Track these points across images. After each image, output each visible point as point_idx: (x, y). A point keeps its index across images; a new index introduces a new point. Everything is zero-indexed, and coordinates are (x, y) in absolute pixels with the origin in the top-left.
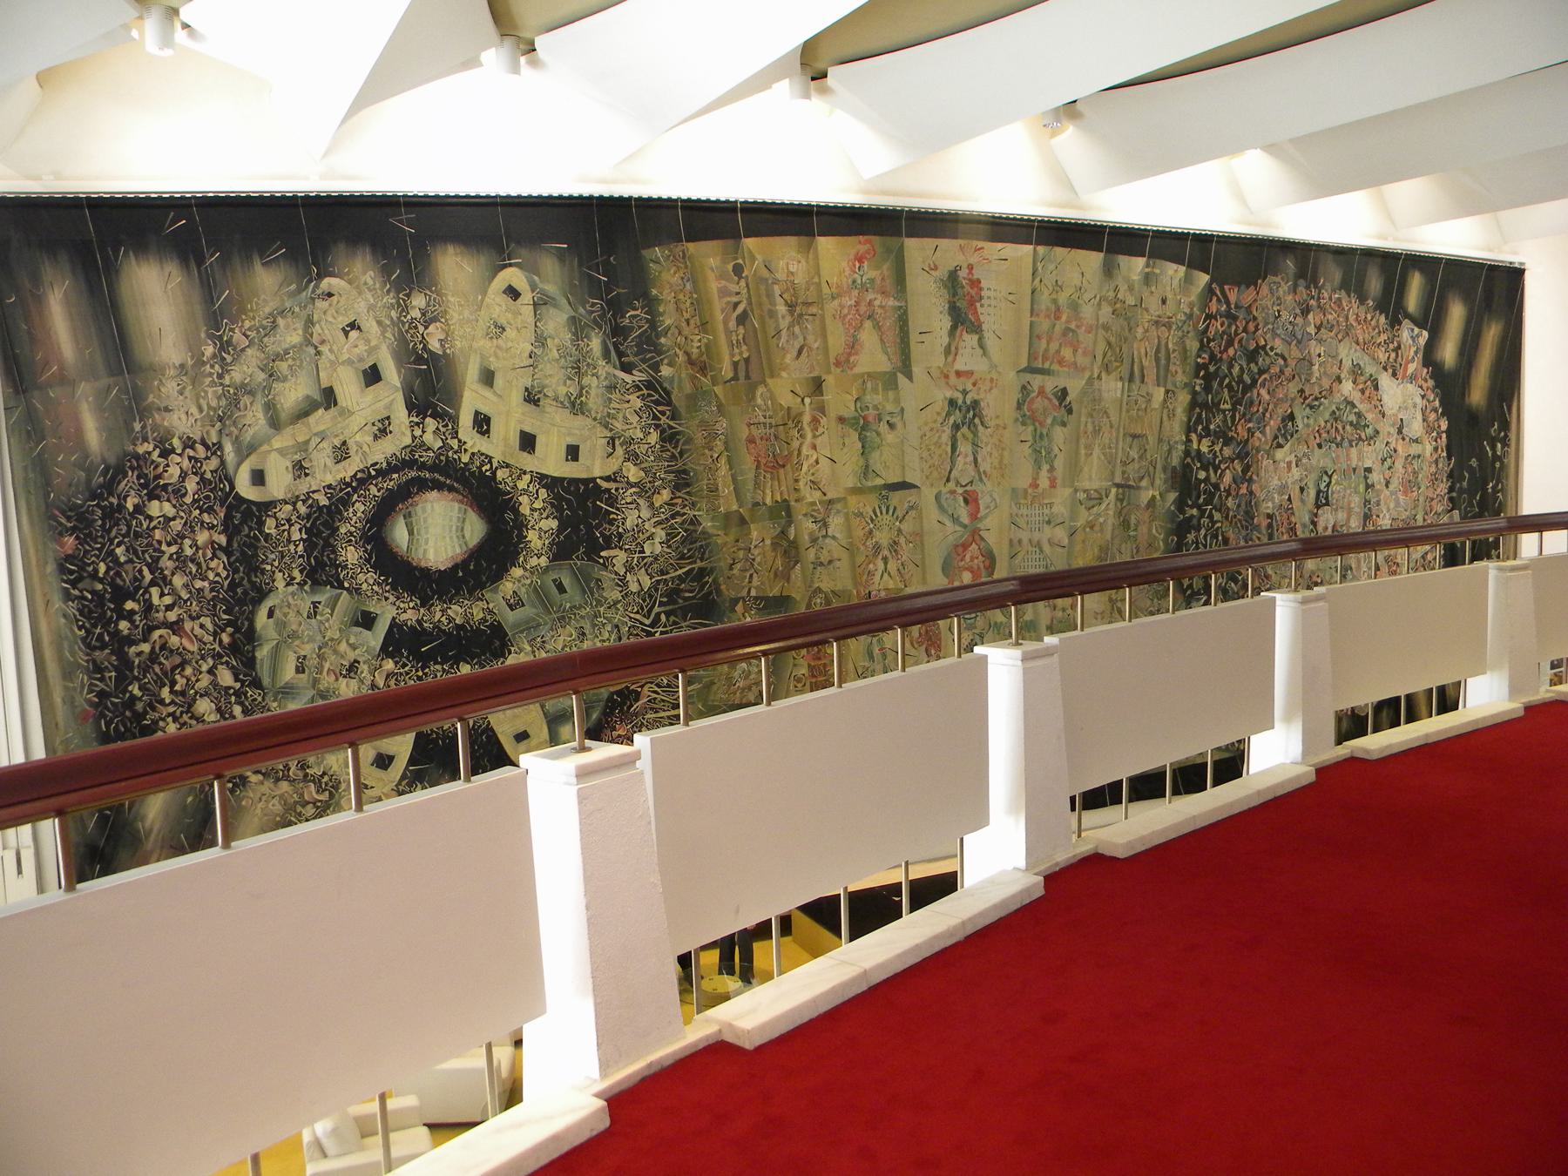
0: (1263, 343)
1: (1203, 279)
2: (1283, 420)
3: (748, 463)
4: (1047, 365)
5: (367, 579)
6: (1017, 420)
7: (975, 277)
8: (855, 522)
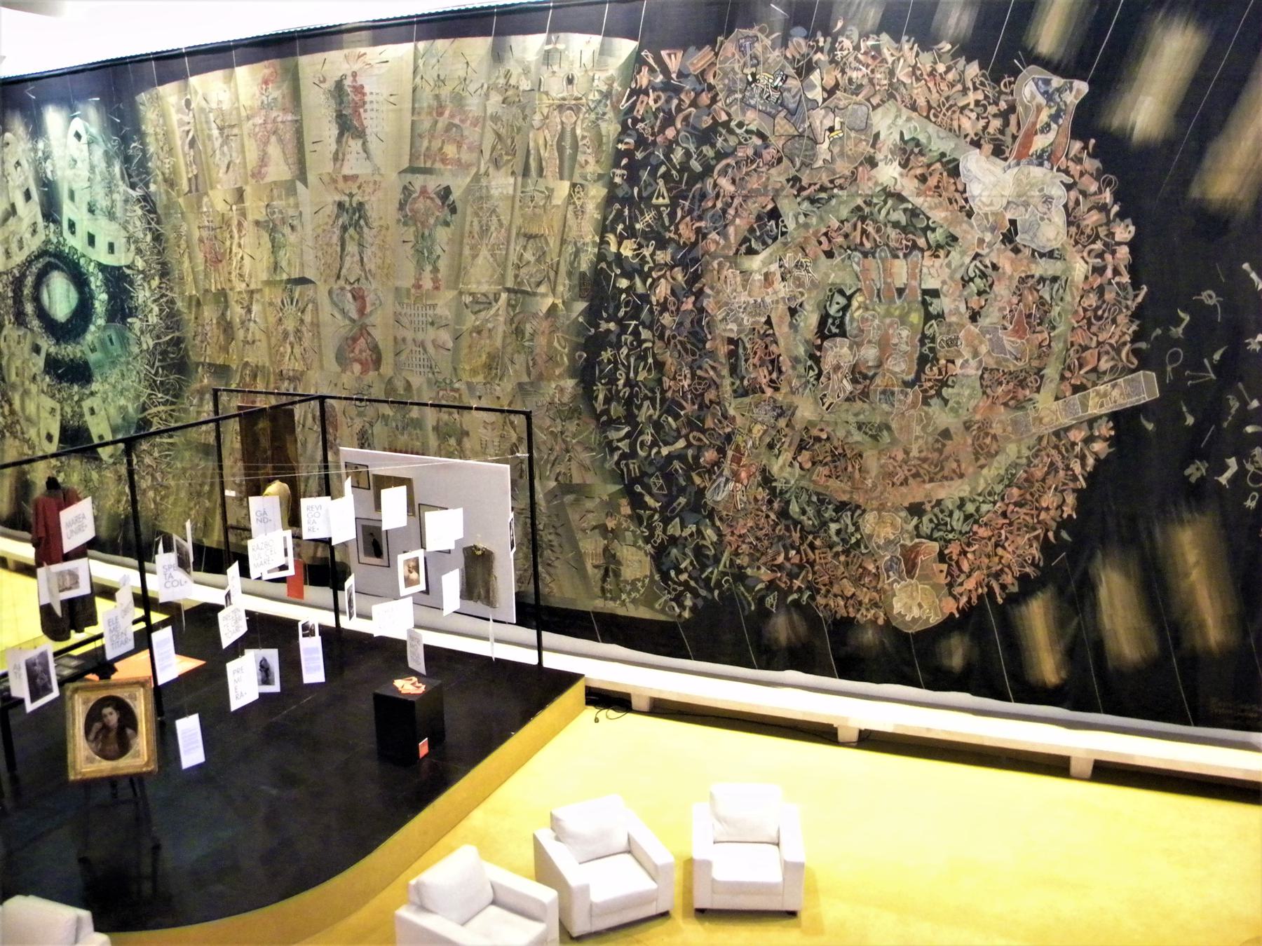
0: (724, 117)
1: (625, 47)
2: (759, 218)
3: (200, 257)
4: (428, 165)
6: (399, 221)
7: (359, 83)
8: (269, 310)
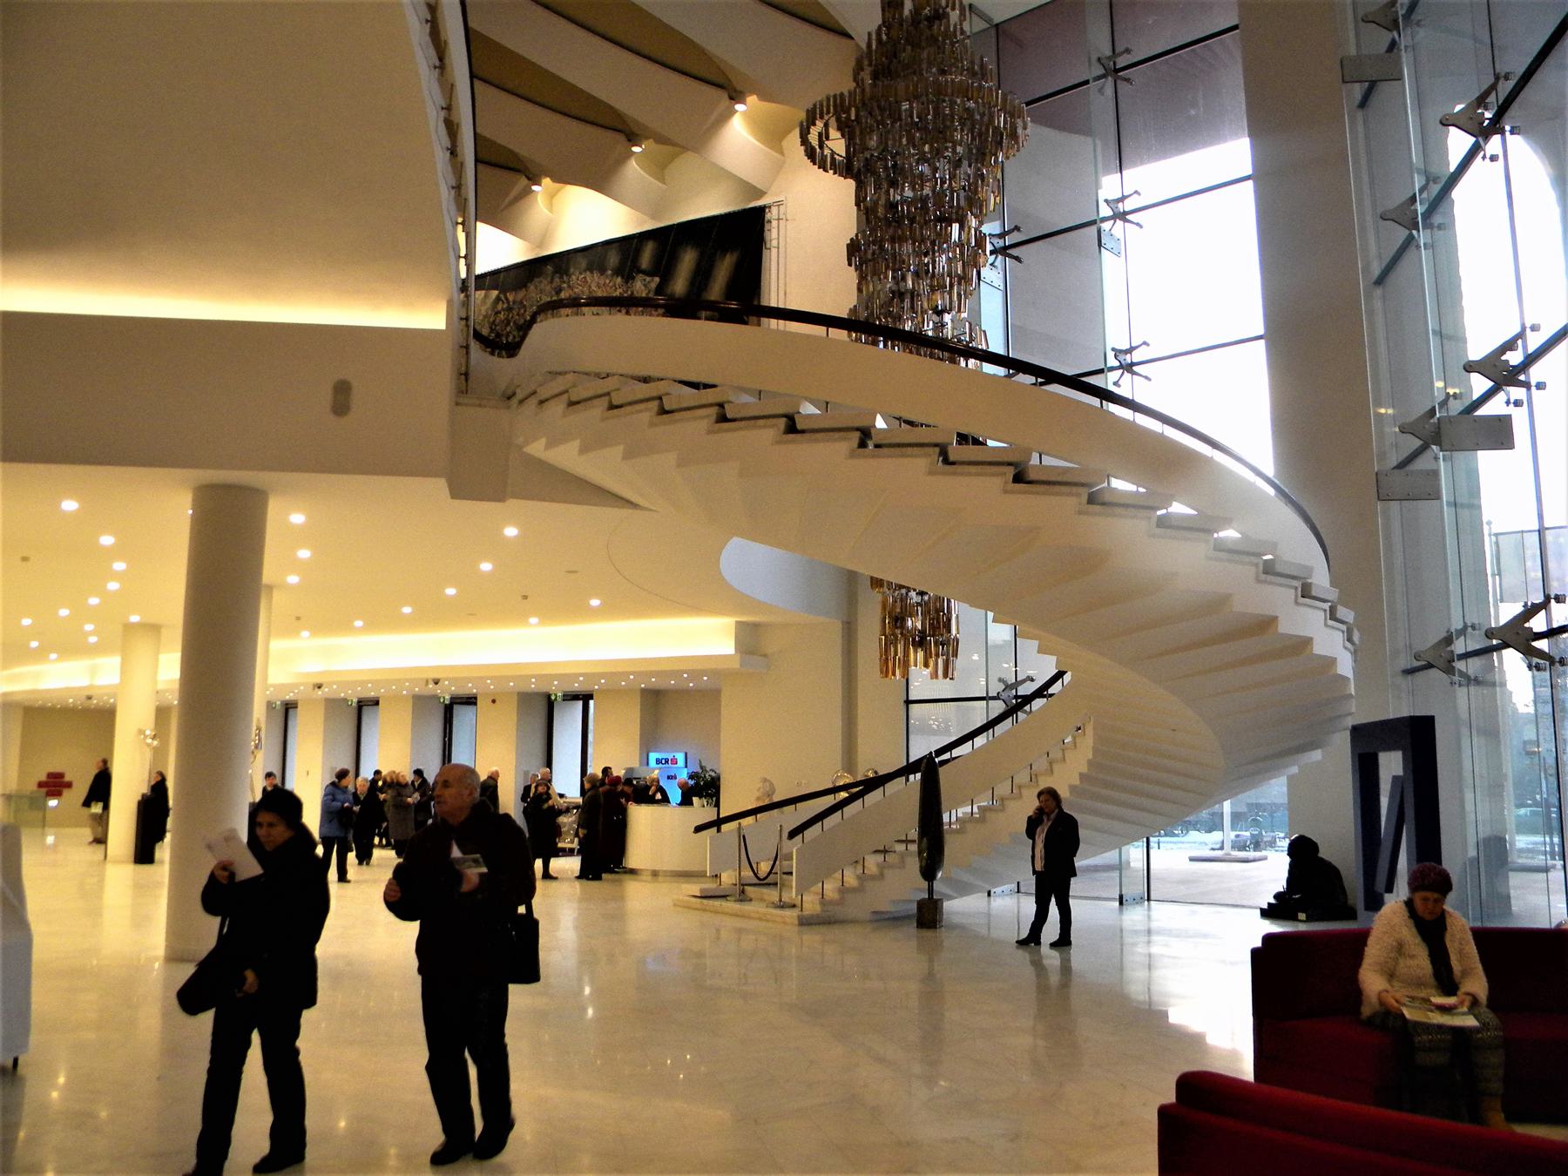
1: (495, 293)
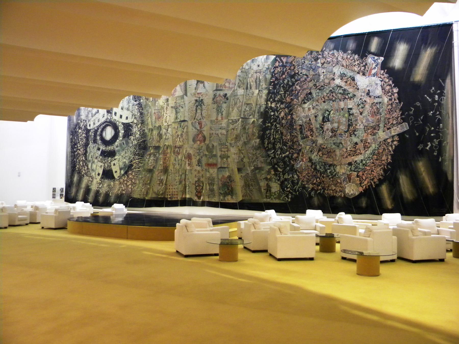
3: (154, 118)
4: (221, 88)
5: (100, 142)
6: (212, 103)
